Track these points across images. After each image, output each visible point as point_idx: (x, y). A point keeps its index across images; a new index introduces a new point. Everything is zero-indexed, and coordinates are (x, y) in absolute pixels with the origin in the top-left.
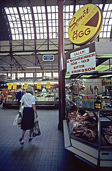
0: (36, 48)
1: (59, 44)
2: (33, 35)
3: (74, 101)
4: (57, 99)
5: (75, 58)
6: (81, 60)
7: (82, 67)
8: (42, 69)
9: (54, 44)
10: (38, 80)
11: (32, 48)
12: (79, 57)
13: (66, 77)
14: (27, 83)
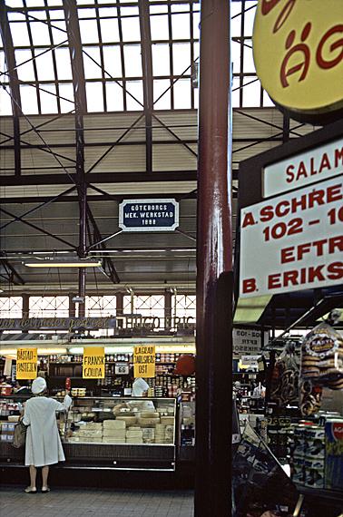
0: (80, 160)
1: (201, 142)
2: (67, 91)
3: (279, 446)
4: (187, 434)
5: (293, 195)
6: (328, 207)
7: (331, 251)
8: (115, 278)
9: (179, 141)
10: (92, 333)
11: (61, 162)
12: (318, 187)
13: (239, 317)
14: (30, 349)
